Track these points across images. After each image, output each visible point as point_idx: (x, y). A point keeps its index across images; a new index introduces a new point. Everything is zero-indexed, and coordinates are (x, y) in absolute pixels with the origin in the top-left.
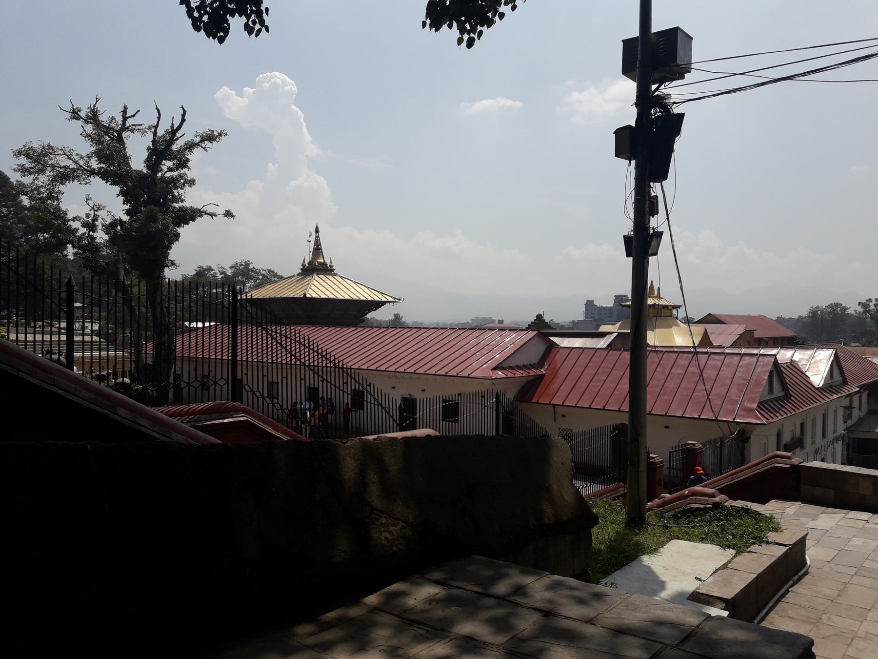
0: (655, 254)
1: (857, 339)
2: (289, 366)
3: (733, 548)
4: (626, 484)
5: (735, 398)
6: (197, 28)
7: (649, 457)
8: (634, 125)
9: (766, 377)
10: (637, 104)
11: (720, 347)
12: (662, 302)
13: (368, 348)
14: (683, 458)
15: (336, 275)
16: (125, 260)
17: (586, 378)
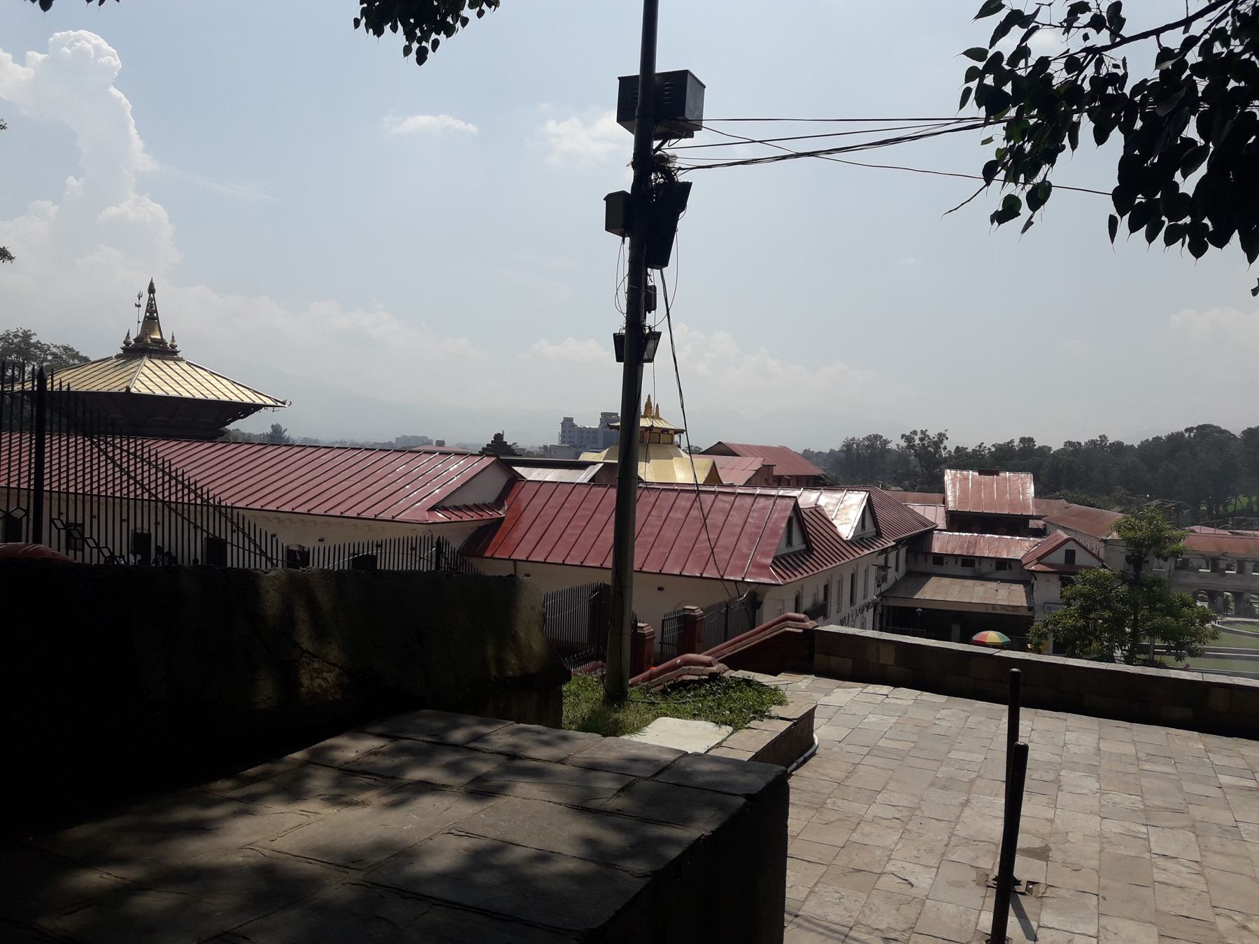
0: (651, 360)
1: (898, 482)
2: (103, 500)
4: (604, 661)
5: (745, 550)
7: (635, 627)
8: (629, 191)
9: (784, 525)
10: (635, 165)
11: (731, 486)
12: (657, 424)
13: (233, 475)
14: (679, 628)
15: (181, 360)
17: (559, 524)
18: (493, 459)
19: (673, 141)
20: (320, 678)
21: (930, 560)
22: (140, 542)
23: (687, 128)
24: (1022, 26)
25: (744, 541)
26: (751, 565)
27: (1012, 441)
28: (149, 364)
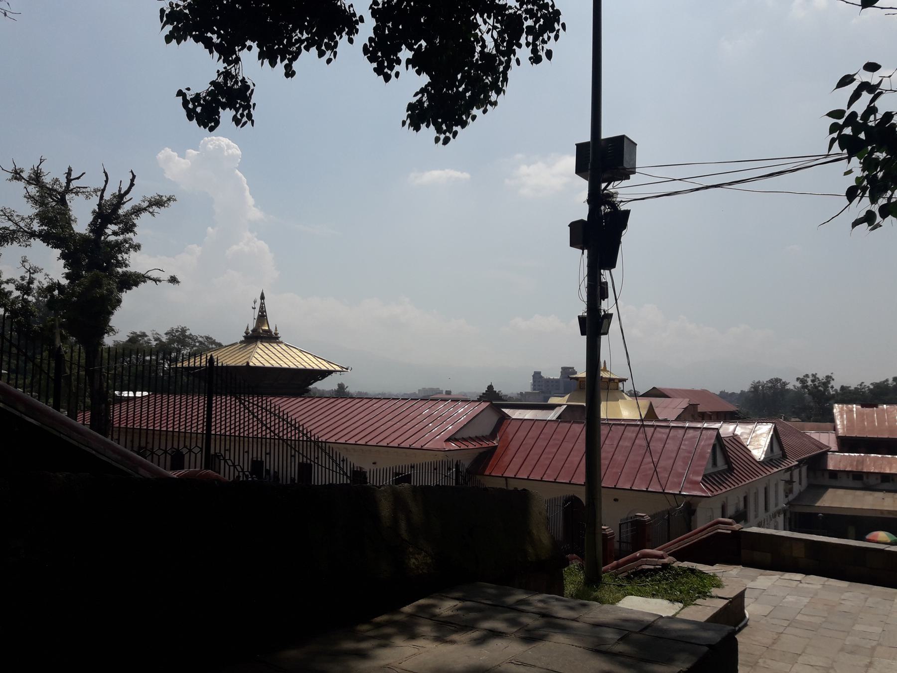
0: (606, 333)
1: (797, 414)
2: (232, 438)
3: (681, 602)
5: (680, 470)
6: (190, 118)
9: (709, 451)
10: (589, 201)
11: (665, 420)
12: (613, 376)
13: (317, 419)
15: (281, 342)
16: (62, 325)
17: (537, 451)
18: (488, 404)
19: (616, 183)
20: (417, 561)
21: (827, 475)
22: (257, 466)
23: (625, 173)
24: (870, 92)
25: (679, 463)
26: (686, 482)
27: (887, 380)
28: (261, 346)
